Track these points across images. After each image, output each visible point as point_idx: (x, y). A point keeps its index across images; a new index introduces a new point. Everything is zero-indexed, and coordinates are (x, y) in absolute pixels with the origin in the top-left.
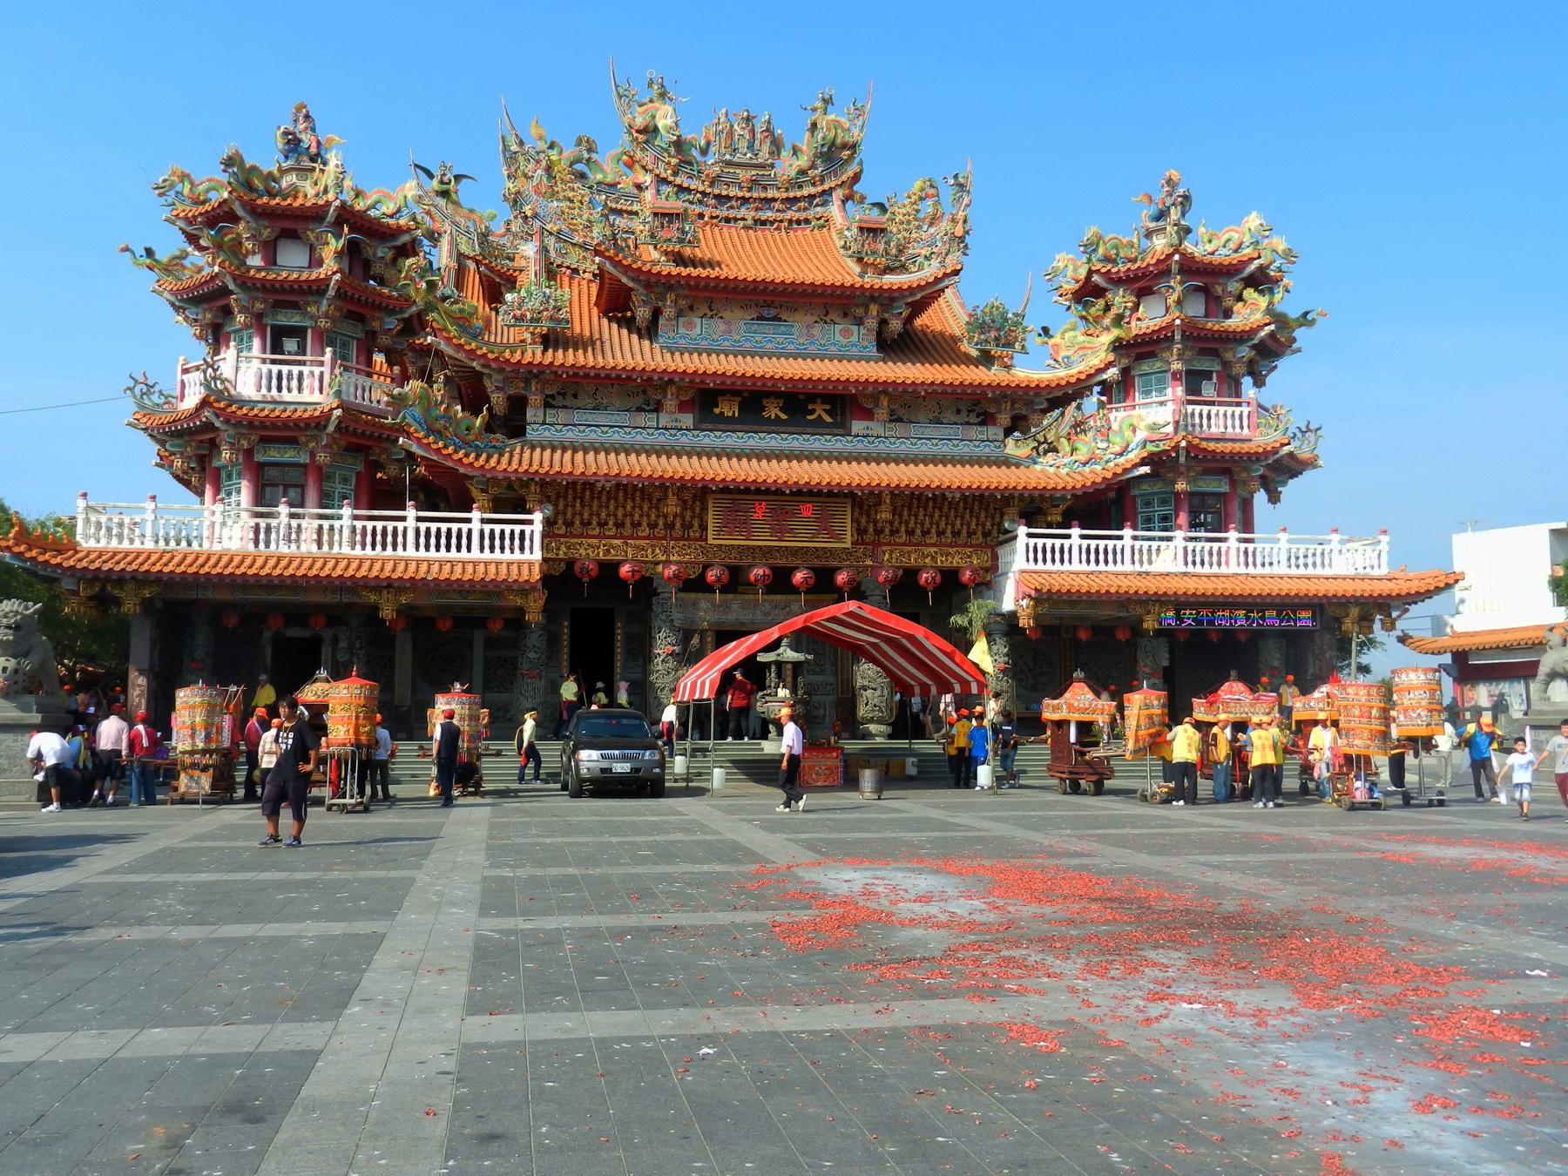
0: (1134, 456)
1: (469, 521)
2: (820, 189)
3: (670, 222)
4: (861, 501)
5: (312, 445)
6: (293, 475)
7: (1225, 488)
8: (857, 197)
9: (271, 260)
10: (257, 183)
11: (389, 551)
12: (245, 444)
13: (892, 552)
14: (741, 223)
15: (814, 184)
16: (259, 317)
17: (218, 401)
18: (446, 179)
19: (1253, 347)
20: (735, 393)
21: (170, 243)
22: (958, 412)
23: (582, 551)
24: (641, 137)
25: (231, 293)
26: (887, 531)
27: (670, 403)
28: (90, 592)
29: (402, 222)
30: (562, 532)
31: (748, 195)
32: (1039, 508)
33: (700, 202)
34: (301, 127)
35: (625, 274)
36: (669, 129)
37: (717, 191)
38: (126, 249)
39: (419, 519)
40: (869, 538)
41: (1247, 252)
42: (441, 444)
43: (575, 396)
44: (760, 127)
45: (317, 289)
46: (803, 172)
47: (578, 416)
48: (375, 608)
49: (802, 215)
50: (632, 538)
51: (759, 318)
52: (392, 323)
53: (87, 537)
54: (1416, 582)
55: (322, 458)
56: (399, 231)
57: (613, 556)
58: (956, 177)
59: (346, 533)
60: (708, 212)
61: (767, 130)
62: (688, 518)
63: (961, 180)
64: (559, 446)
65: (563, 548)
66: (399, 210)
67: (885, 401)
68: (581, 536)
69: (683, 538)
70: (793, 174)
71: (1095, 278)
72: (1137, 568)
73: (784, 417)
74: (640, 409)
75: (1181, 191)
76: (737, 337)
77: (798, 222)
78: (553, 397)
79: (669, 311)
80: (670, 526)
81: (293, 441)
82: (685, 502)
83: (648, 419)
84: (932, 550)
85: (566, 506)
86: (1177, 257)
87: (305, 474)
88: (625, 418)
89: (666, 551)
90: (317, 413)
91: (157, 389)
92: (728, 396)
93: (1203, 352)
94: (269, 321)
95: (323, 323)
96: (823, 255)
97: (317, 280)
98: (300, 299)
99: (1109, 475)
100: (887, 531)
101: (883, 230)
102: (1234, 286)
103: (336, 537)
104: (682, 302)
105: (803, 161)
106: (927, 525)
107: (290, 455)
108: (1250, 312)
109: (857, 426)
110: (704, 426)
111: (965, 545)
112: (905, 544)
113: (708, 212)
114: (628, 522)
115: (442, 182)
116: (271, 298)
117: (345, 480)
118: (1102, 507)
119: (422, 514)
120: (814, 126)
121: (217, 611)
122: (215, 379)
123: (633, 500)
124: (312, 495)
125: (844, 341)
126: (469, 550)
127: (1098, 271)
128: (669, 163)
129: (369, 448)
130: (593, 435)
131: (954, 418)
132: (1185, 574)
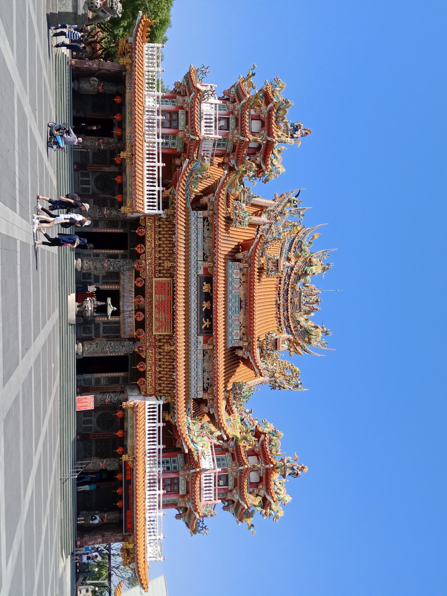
0: (192, 446)
1: (159, 489)
2: (292, 330)
3: (275, 266)
4: (171, 339)
5: (185, 130)
6: (175, 124)
7: (181, 493)
9: (253, 118)
10: (281, 112)
11: (146, 192)
13: (152, 353)
14: (278, 299)
15: (294, 327)
16: (232, 113)
17: (200, 95)
18: (295, 202)
19: (238, 502)
20: (212, 290)
22: (208, 379)
23: (149, 232)
24: (308, 260)
25: (240, 102)
26: (160, 350)
28: (127, 46)
29: (270, 166)
30: (156, 243)
31: (289, 301)
33: (285, 283)
34: (303, 132)
35: (254, 247)
36: (311, 271)
37: (290, 289)
39: (159, 167)
40: (158, 344)
41: (276, 496)
42: (187, 175)
43: (208, 230)
44: (315, 306)
45: (243, 134)
46: (299, 322)
48: (124, 149)
49: (282, 323)
50: (155, 251)
51: (241, 300)
52: (233, 162)
54: (143, 566)
55: (180, 134)
56: (266, 165)
57: (148, 244)
58: (301, 384)
59: (153, 140)
60: (282, 286)
61: (314, 309)
62: (163, 272)
63: (300, 386)
64: (188, 228)
65: (150, 224)
66: (274, 165)
67: (211, 347)
68: (155, 231)
69: (155, 270)
70: (298, 319)
71: (263, 436)
72: (147, 497)
73: (204, 309)
74: (204, 254)
75: (300, 472)
77: (280, 321)
78: (207, 221)
79: (241, 265)
80: (160, 265)
81: (187, 123)
82: (169, 352)
84: (153, 370)
85: (166, 225)
86: (272, 466)
87: (175, 128)
89: (150, 264)
90: (197, 131)
91: (204, 76)
92: (210, 288)
93: (236, 480)
94: (231, 116)
95: (230, 136)
96: (265, 322)
97: (246, 133)
98: (239, 127)
99: (184, 436)
100: (160, 350)
101: (276, 348)
102: (262, 492)
103: (151, 137)
104: (245, 270)
105: (303, 323)
106: (163, 366)
107: (182, 122)
108: (252, 500)
109: (201, 338)
110: (199, 278)
111: (155, 383)
112: (155, 358)
113: (281, 286)
114: (161, 249)
115: (294, 201)
116: (239, 117)
118: (171, 438)
120: (317, 327)
121: (122, 95)
122: (208, 95)
123: (169, 250)
127: (265, 436)
128: (299, 271)
129: (186, 153)
132: (145, 472)
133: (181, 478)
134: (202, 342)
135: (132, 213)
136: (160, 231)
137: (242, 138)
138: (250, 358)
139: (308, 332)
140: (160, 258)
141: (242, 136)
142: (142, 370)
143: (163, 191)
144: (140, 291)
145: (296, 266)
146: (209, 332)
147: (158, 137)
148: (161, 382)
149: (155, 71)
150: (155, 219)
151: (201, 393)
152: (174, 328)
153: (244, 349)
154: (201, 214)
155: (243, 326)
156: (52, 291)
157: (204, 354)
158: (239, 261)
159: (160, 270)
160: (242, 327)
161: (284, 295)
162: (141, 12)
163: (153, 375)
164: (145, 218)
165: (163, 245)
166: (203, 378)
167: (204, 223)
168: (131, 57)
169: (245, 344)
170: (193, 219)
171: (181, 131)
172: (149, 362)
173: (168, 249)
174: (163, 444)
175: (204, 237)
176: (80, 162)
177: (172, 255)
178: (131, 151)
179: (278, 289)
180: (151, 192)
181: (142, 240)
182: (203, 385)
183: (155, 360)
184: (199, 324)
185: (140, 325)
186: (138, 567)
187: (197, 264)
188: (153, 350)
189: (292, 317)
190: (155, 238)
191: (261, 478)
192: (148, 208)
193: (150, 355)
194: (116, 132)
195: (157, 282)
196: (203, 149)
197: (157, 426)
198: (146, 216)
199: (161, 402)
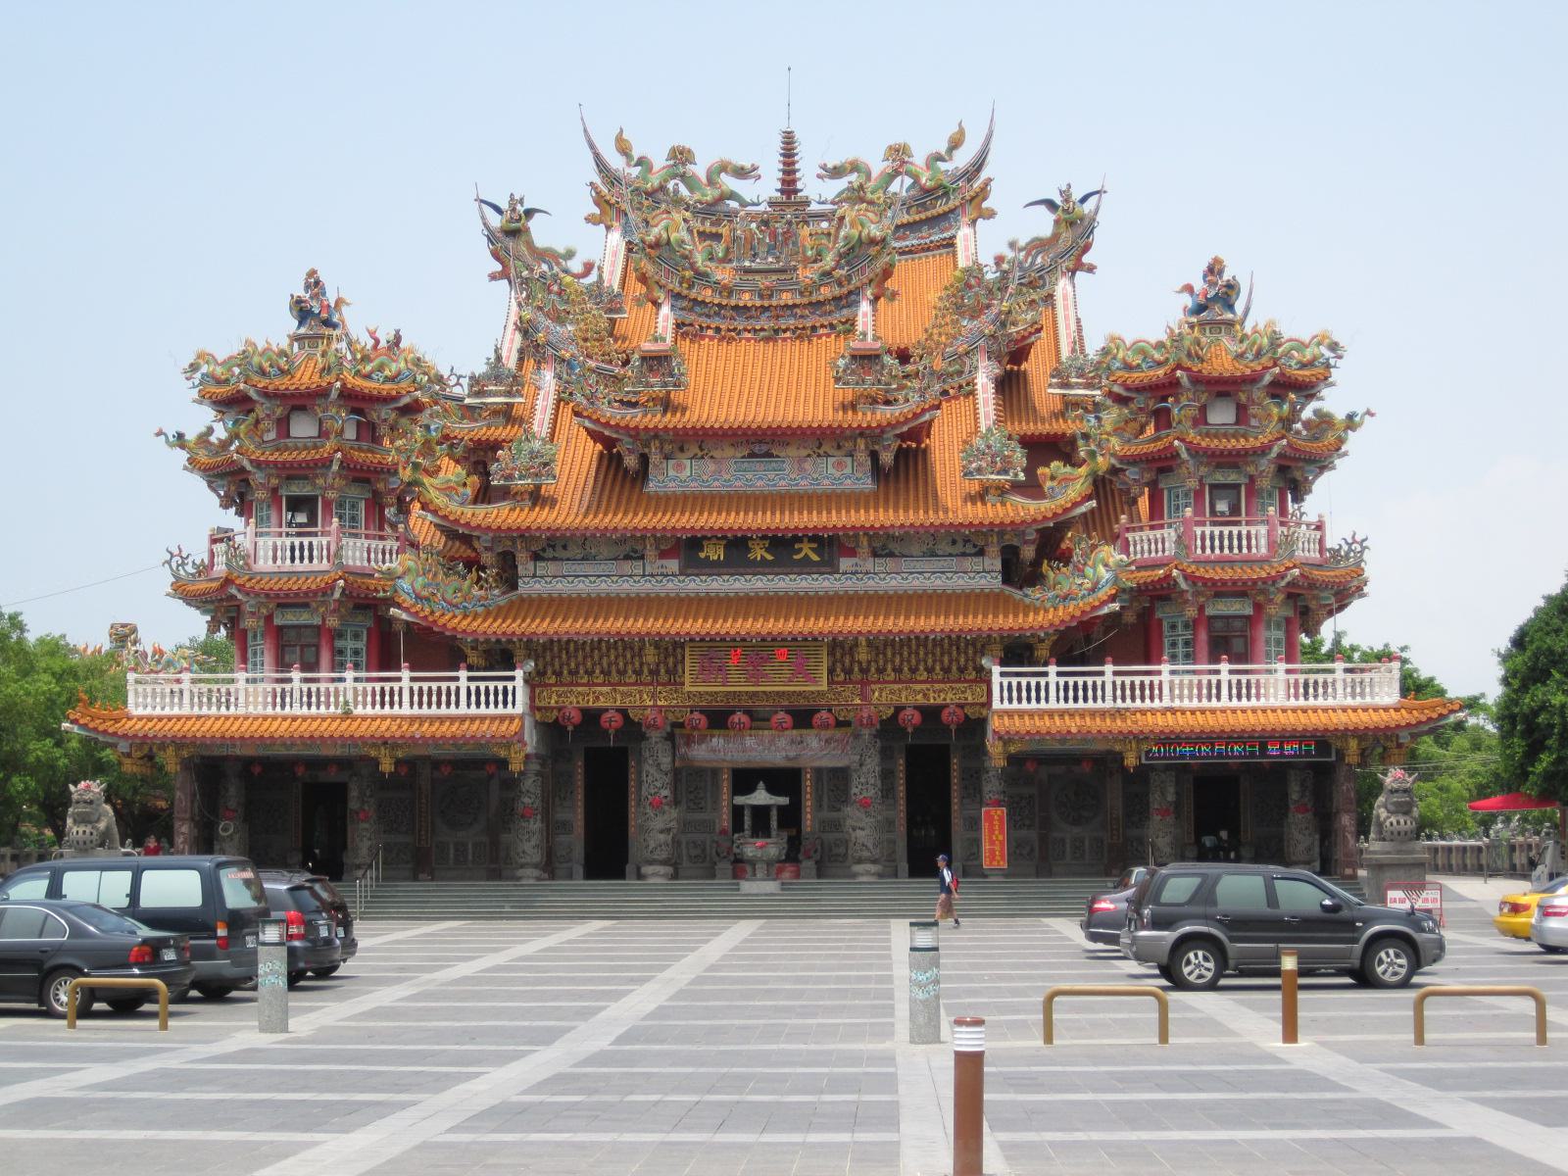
0: (1102, 594)
4: (840, 648)
5: (322, 610)
8: (888, 293)
12: (264, 611)
13: (881, 690)
16: (275, 490)
21: (200, 419)
22: (954, 542)
27: (650, 552)
28: (139, 754)
32: (1018, 652)
33: (717, 314)
37: (733, 302)
38: (160, 433)
40: (857, 675)
43: (565, 547)
47: (566, 568)
51: (752, 455)
53: (137, 705)
55: (333, 622)
57: (602, 703)
59: (296, 695)
65: (554, 697)
68: (571, 684)
69: (669, 683)
73: (769, 557)
74: (627, 557)
76: (727, 477)
79: (655, 458)
80: (654, 673)
81: (306, 605)
83: (637, 567)
84: (924, 686)
87: (319, 635)
88: (611, 567)
89: (653, 696)
91: (190, 560)
102: (1258, 393)
106: (914, 662)
107: (304, 618)
109: (845, 564)
110: (689, 571)
111: (959, 681)
112: (895, 682)
117: (356, 636)
119: (1290, 666)
124: (325, 658)
125: (837, 474)
126: (1103, 700)
130: (581, 586)
131: (950, 549)
133: (1209, 611)
134: (853, 560)
135: (521, 741)
136: (570, 672)
137: (335, 467)
138: (898, 432)
139: (853, 248)
140: (638, 673)
141: (330, 466)
142: (917, 718)
143: (470, 668)
144: (718, 719)
145: (671, 286)
146: (831, 547)
147: (341, 680)
148: (954, 668)
149: (195, 697)
150: (540, 685)
151: (987, 561)
152: (811, 641)
153: (877, 447)
154: (525, 566)
155: (819, 447)
156: (984, 981)
157: (887, 555)
158: (644, 460)
159: (668, 672)
160: (821, 452)
161: (751, 317)
162: (65, 725)
163: (937, 686)
164: (539, 709)
165: (605, 665)
166: (950, 555)
167: (548, 560)
168: (163, 747)
169: (863, 447)
170: (537, 586)
171: (324, 620)
172: (904, 698)
173: (605, 661)
174: (1102, 664)
175: (583, 559)
176: (410, 866)
177: (628, 647)
178: (374, 745)
179: (726, 337)
180: (473, 698)
181: (591, 716)
182: (970, 555)
183: (900, 681)
184: (808, 570)
185: (803, 718)
186: (1409, 725)
187: (652, 576)
188: (873, 686)
189: (811, 293)
190: (587, 685)
191: (1221, 395)
192: (510, 705)
193: (884, 697)
194: (332, 775)
195: (694, 683)
196: (366, 563)
197: (1057, 679)
198: (533, 707)
199: (996, 670)
